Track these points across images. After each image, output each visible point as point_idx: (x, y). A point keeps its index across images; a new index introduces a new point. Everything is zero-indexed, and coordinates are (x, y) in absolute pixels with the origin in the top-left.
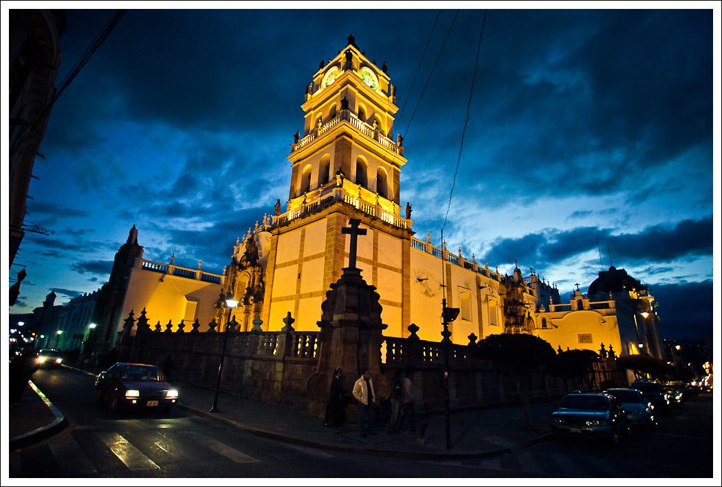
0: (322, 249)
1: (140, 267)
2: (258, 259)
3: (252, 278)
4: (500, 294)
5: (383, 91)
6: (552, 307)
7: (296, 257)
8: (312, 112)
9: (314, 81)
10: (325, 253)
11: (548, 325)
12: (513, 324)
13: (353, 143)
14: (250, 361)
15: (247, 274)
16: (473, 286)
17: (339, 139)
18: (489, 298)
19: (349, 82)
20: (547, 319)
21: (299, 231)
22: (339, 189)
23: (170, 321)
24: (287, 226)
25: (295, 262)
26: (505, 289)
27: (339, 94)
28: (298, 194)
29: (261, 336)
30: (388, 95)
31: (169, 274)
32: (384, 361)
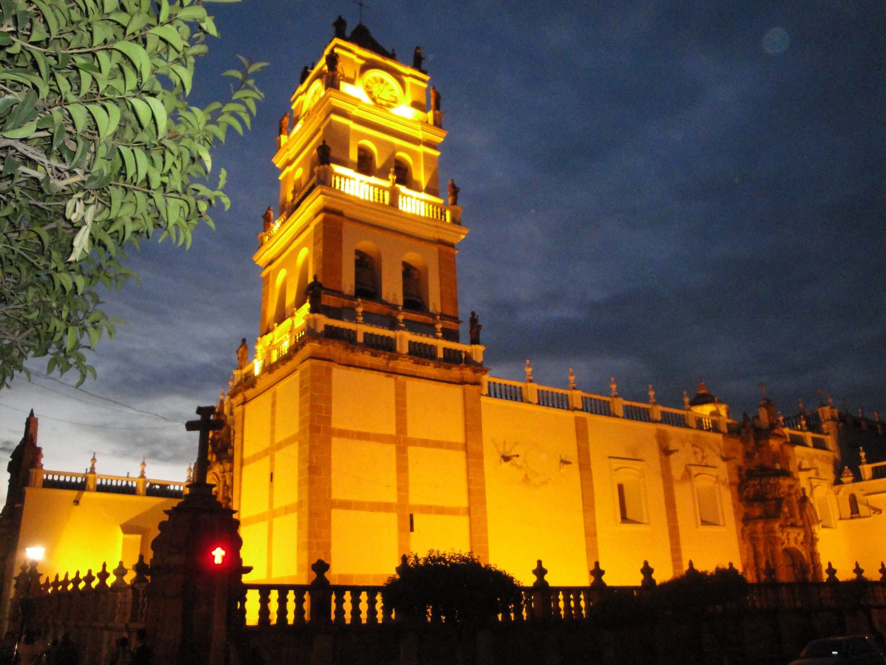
0: (295, 430)
1: (39, 483)
4: (725, 459)
6: (866, 469)
11: (863, 509)
12: (760, 517)
16: (652, 453)
18: (695, 471)
20: (859, 497)
21: (268, 396)
23: (540, 562)
24: (253, 387)
26: (740, 446)
29: (119, 594)
31: (89, 490)
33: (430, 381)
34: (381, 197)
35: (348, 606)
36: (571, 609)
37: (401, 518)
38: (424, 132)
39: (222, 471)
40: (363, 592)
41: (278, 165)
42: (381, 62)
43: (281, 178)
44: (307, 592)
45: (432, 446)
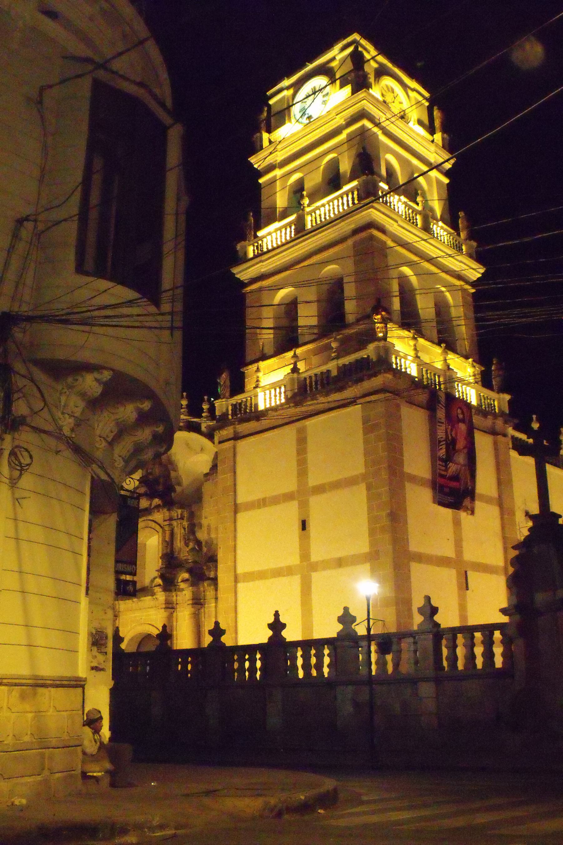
2: (175, 491)
3: (168, 533)
5: (420, 122)
7: (291, 485)
8: (278, 173)
9: (271, 102)
10: (364, 477)
14: (350, 688)
15: (153, 525)
17: (358, 237)
19: (363, 115)
22: (381, 344)
23: (277, 614)
25: (288, 497)
27: (343, 136)
28: (269, 350)
30: (432, 131)
32: (258, 679)
35: (460, 652)
38: (437, 155)
39: (167, 518)
42: (391, 69)
43: (261, 181)
44: (299, 649)
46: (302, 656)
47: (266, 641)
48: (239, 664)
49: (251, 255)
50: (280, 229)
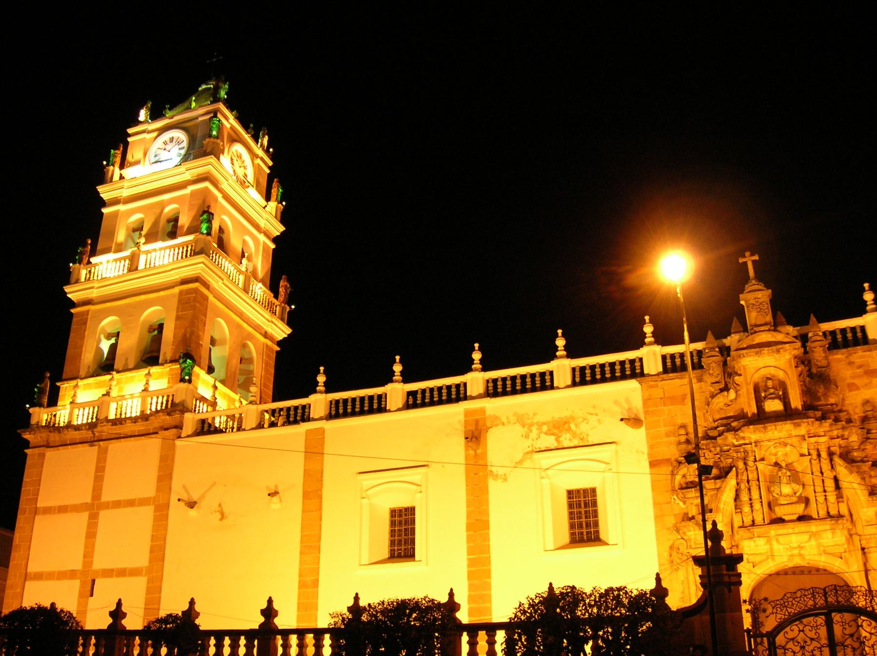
8: (121, 208)
13: (211, 298)
23: (270, 601)
33: (128, 439)
34: (237, 278)
36: (126, 645)
37: (83, 584)
40: (480, 632)
41: (105, 196)
45: (124, 507)
46: (215, 645)
47: (105, 627)
48: (83, 649)
49: (83, 279)
50: (165, 248)
